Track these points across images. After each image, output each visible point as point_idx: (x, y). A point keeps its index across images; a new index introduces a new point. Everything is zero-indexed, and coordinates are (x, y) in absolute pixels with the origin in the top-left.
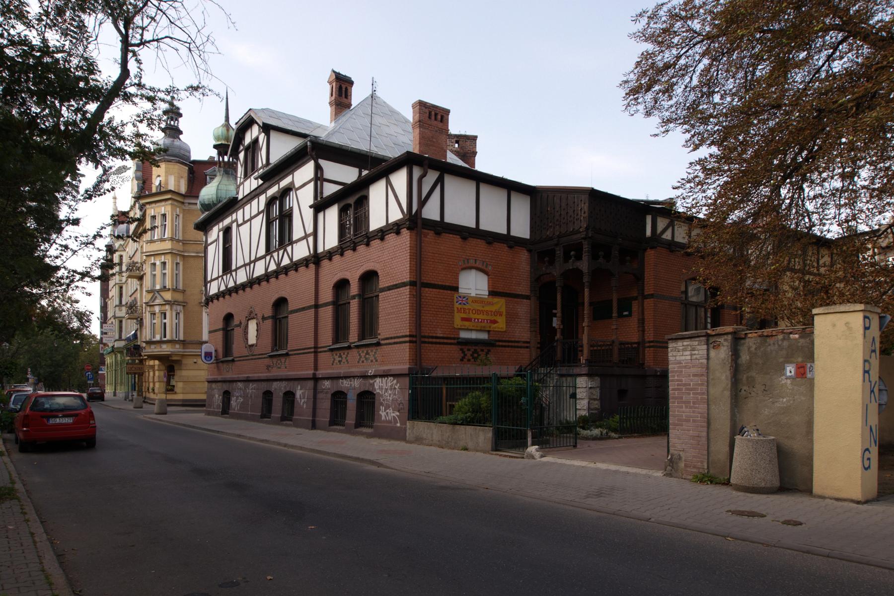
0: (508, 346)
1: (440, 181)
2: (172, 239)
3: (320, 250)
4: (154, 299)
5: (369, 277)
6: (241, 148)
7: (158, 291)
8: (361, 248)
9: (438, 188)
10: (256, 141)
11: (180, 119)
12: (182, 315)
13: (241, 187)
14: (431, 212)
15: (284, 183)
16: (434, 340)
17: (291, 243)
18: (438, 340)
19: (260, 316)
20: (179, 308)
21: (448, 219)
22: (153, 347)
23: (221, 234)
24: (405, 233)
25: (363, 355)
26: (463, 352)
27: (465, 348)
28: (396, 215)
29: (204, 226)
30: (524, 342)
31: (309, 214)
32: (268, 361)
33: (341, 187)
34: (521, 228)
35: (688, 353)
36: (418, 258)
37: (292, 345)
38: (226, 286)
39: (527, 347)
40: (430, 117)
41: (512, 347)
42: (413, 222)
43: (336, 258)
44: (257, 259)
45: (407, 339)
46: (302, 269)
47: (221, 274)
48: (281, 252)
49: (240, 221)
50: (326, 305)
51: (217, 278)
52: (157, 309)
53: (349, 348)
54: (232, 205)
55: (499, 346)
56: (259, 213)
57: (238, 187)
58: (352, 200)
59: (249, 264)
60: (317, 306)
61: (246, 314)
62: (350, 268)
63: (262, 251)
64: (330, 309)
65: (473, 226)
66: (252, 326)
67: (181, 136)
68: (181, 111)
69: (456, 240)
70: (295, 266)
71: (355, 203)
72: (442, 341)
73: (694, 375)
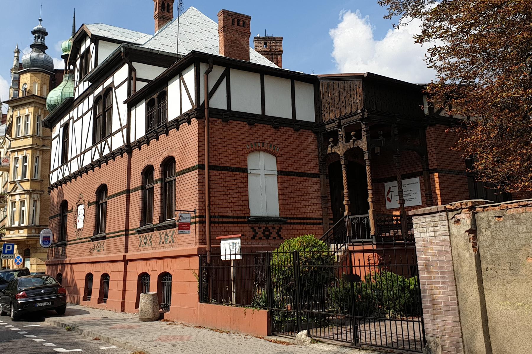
0: (300, 223)
1: (226, 75)
2: (33, 136)
3: (132, 140)
4: (15, 189)
5: (169, 163)
6: (79, 56)
7: (20, 182)
8: (162, 137)
9: (225, 81)
10: (88, 50)
11: (46, 37)
12: (38, 203)
13: (77, 89)
14: (218, 102)
15: (106, 84)
16: (224, 220)
17: (111, 135)
18: (228, 220)
19: (86, 202)
20: (36, 196)
21: (234, 108)
22: (12, 232)
23: (62, 129)
24: (194, 121)
25: (163, 236)
26: (254, 230)
27: (256, 227)
28: (187, 107)
29: (50, 124)
30: (317, 219)
31: (124, 108)
32: (91, 244)
33: (145, 84)
34: (306, 113)
35: (431, 229)
36: (207, 144)
37: (109, 228)
38: (63, 176)
39: (320, 224)
40: (233, 23)
41: (304, 224)
42: (200, 112)
43: (144, 146)
44: (86, 151)
45: (197, 220)
46: (118, 158)
47: (60, 165)
48: (103, 143)
49: (75, 118)
50: (136, 189)
51: (57, 169)
52: (17, 198)
53: (152, 230)
54: (69, 104)
55: (291, 223)
56: (89, 110)
57: (75, 90)
58: (153, 96)
59: (80, 155)
60: (128, 191)
61: (76, 200)
62: (152, 155)
63: (90, 144)
64: (139, 193)
65: (259, 112)
66: (81, 208)
67: (46, 51)
68: (47, 31)
69: (245, 126)
70: (113, 155)
71: (157, 97)
72: (232, 220)
73: (439, 253)
